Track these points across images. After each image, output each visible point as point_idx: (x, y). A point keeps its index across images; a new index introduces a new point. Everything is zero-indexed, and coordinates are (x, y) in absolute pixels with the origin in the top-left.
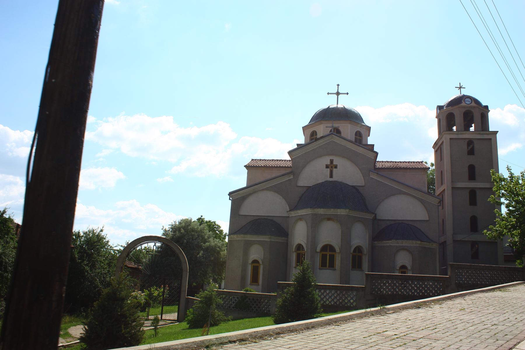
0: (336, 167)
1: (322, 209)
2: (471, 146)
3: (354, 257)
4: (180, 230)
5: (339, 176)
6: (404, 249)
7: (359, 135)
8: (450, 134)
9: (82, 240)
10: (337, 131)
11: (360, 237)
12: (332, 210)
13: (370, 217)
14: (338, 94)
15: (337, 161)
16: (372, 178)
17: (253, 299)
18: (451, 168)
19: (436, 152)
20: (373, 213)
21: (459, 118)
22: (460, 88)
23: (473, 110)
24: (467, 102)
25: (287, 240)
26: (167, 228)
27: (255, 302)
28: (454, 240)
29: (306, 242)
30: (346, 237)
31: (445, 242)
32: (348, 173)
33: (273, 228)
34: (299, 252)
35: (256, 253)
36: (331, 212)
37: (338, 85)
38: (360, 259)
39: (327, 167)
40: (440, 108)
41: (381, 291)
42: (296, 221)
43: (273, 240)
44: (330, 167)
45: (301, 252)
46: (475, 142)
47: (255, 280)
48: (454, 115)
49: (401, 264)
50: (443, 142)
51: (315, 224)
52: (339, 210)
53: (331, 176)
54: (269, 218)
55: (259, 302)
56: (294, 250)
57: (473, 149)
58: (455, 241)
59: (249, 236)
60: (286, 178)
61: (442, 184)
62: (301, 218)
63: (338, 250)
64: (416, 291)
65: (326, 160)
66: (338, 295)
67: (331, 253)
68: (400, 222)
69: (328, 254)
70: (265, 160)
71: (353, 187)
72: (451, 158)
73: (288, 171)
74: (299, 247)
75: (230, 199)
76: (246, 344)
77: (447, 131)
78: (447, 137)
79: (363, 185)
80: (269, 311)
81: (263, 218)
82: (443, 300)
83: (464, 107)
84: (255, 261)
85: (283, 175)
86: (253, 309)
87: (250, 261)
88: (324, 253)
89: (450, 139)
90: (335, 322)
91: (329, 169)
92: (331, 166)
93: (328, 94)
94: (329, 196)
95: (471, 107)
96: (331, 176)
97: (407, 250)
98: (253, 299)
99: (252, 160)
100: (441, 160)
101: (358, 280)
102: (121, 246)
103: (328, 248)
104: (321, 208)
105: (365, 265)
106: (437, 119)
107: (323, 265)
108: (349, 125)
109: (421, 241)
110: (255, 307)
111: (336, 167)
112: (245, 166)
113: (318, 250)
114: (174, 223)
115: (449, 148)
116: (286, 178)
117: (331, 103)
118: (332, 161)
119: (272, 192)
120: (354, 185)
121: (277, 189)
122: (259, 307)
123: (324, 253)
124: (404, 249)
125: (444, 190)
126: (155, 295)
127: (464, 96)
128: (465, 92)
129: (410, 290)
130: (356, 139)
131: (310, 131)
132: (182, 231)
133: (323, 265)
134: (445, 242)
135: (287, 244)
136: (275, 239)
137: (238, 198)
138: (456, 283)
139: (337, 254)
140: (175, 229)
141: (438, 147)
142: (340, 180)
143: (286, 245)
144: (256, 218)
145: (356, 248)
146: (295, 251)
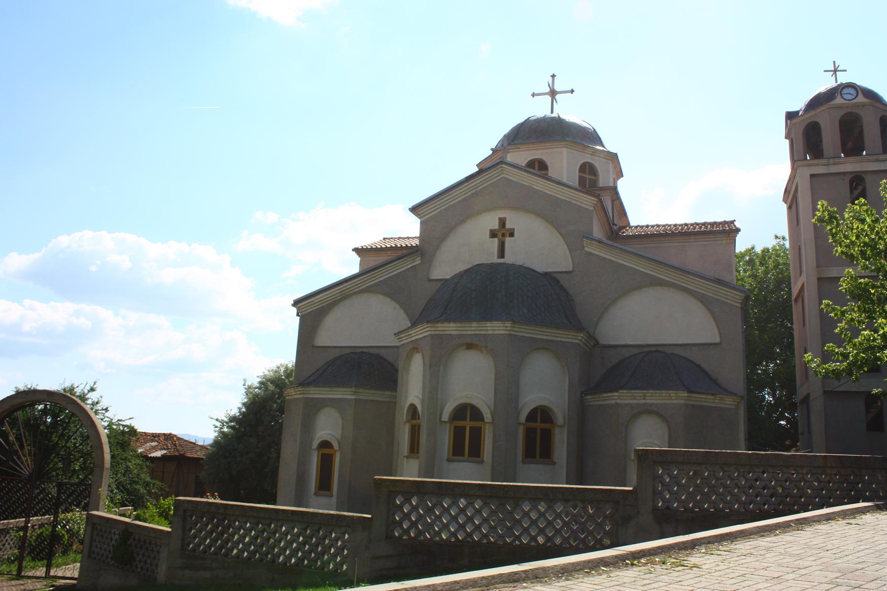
0: (512, 235)
1: (452, 325)
3: (530, 434)
5: (518, 253)
6: (649, 411)
7: (588, 170)
10: (539, 167)
11: (545, 384)
12: (474, 324)
14: (553, 93)
16: (590, 253)
17: (139, 541)
18: (816, 238)
19: (790, 208)
20: (579, 328)
21: (830, 137)
22: (835, 71)
23: (860, 112)
24: (845, 96)
25: (395, 397)
26: (255, 381)
29: (492, 404)
30: (508, 388)
31: (808, 396)
32: (537, 246)
33: (371, 370)
36: (472, 328)
37: (553, 76)
38: (547, 437)
39: (493, 234)
40: (790, 116)
42: (409, 357)
43: (362, 397)
44: (500, 235)
47: (324, 485)
52: (488, 324)
53: (502, 254)
54: (371, 351)
62: (415, 348)
63: (487, 416)
65: (491, 221)
67: (546, 426)
68: (654, 349)
69: (468, 424)
71: (546, 274)
74: (413, 409)
75: (298, 315)
78: (806, 172)
79: (571, 269)
82: (686, 549)
83: (840, 107)
84: (325, 444)
88: (461, 423)
89: (812, 176)
90: (785, 527)
91: (496, 240)
92: (502, 233)
93: (533, 95)
94: (496, 295)
95: (857, 105)
96: (502, 254)
97: (659, 415)
98: (145, 541)
102: (217, 420)
104: (449, 322)
106: (787, 141)
109: (690, 391)
111: (512, 235)
112: (357, 250)
113: (446, 417)
117: (540, 109)
118: (502, 222)
119: (381, 297)
120: (550, 270)
121: (392, 289)
123: (461, 423)
124: (649, 411)
126: (415, 498)
127: (842, 84)
128: (843, 78)
130: (582, 180)
132: (271, 387)
133: (457, 451)
134: (808, 396)
135: (395, 403)
136: (367, 395)
137: (313, 310)
138: (655, 509)
143: (391, 407)
144: (347, 351)
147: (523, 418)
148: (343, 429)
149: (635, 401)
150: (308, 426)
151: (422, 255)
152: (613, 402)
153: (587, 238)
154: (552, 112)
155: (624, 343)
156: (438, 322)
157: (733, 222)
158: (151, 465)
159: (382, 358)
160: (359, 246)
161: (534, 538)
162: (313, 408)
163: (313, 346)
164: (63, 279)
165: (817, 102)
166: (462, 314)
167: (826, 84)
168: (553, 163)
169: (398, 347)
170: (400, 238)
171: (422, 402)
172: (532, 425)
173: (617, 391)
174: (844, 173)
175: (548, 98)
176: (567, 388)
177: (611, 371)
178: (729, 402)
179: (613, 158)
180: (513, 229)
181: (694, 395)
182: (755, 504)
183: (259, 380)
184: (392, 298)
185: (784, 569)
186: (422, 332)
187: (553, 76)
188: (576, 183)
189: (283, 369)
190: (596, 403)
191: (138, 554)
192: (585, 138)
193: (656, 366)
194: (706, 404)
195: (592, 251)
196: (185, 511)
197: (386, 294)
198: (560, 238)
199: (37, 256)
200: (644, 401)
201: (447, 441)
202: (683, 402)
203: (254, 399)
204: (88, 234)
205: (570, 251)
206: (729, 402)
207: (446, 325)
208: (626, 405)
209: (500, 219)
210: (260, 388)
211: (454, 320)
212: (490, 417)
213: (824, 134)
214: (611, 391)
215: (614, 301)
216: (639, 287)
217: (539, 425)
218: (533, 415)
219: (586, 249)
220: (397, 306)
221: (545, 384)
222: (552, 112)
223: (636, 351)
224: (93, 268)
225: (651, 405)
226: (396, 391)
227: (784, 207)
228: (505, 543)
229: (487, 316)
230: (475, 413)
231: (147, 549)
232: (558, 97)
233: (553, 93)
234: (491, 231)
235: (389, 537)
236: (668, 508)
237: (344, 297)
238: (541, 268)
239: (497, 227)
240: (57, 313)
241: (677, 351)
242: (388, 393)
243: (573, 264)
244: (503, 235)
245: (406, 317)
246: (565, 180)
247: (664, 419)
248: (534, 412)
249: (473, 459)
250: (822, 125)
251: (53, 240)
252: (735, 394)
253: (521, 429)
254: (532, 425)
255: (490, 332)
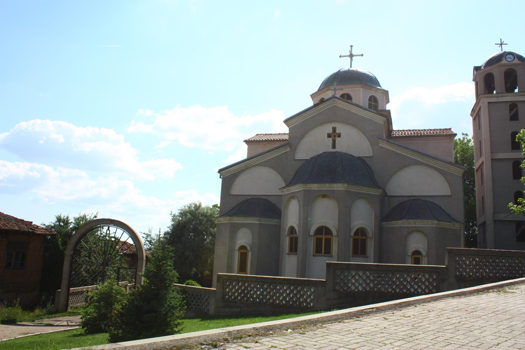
0: (339, 136)
1: (315, 185)
2: (515, 110)
3: (355, 241)
4: (186, 215)
6: (418, 230)
8: (488, 97)
9: (71, 226)
10: (347, 97)
11: (363, 216)
12: (327, 185)
13: (376, 192)
14: (351, 56)
15: (341, 128)
16: (382, 147)
17: (193, 295)
18: (490, 137)
19: (474, 119)
20: (379, 187)
21: (499, 81)
22: (501, 44)
23: (515, 68)
24: (508, 59)
25: (280, 222)
26: (177, 212)
27: (195, 298)
28: (494, 220)
29: (337, 227)
30: (345, 216)
31: (485, 222)
32: (353, 142)
33: (265, 208)
34: (292, 235)
35: (244, 238)
36: (326, 187)
37: (351, 46)
38: (364, 243)
39: (329, 136)
40: (477, 69)
41: (349, 287)
45: (294, 235)
46: (519, 105)
47: (242, 268)
48: (493, 76)
49: (414, 249)
50: (480, 108)
51: (308, 201)
52: (335, 185)
53: (334, 146)
54: (263, 197)
55: (199, 299)
56: (286, 234)
57: (511, 110)
58: (495, 221)
59: (235, 218)
60: (282, 151)
61: (481, 156)
62: (293, 196)
63: (334, 233)
64: (398, 286)
65: (328, 129)
66: (292, 291)
67: (363, 238)
68: (416, 198)
70: (271, 134)
71: (359, 158)
72: (490, 127)
73: (286, 142)
74: (292, 230)
75: (220, 177)
76: (237, 342)
77: (485, 94)
78: (485, 100)
79: (372, 155)
80: (208, 310)
81: (256, 197)
83: (504, 65)
84: (243, 247)
85: (278, 148)
86: (192, 308)
87: (237, 247)
89: (489, 103)
91: (331, 139)
92: (334, 135)
94: (329, 168)
96: (334, 146)
98: (197, 295)
99: (257, 135)
100: (479, 128)
101: (318, 271)
102: (144, 234)
103: (323, 230)
105: (371, 250)
106: (474, 82)
107: (318, 251)
108: (361, 89)
109: (439, 221)
110: (194, 305)
111: (339, 136)
112: (246, 141)
113: (312, 233)
114: (183, 208)
115: (487, 113)
116: (282, 151)
117: (344, 65)
118: (334, 129)
119: (267, 168)
121: (275, 165)
122: (198, 305)
124: (418, 230)
125: (483, 162)
127: (505, 52)
129: (391, 286)
130: (370, 106)
131: (320, 100)
132: (189, 216)
133: (318, 251)
134: (485, 222)
135: (280, 226)
136: (266, 221)
137: (229, 175)
138: (456, 275)
139: (334, 238)
140: (183, 214)
141: (476, 114)
142: (344, 151)
143: (278, 228)
144: (249, 198)
145: (358, 229)
146: (288, 235)
147: (352, 234)
148: (252, 239)
149: (410, 225)
150: (233, 237)
151: (290, 147)
152: (398, 225)
153: (381, 139)
154: (351, 67)
155: (400, 195)
156: (308, 183)
157: (450, 129)
158: (128, 259)
159: (269, 201)
160: (247, 138)
161: (401, 290)
162: (234, 229)
163: (230, 195)
164: (24, 148)
165: (492, 62)
166: (318, 178)
167: (496, 51)
168: (350, 94)
169: (281, 195)
170: (266, 134)
171: (299, 226)
172: (357, 237)
173: (401, 220)
174: (507, 102)
175: (349, 59)
176: (373, 218)
177: (399, 209)
178: (457, 226)
179: (386, 93)
180: (340, 133)
181: (440, 222)
182: (499, 274)
183: (179, 211)
184: (274, 169)
185: (338, 344)
186: (297, 188)
187: (351, 46)
188: (367, 107)
189: (193, 206)
190: (389, 226)
191: (192, 301)
192: (368, 81)
193: (416, 207)
194: (446, 227)
195: (383, 146)
196: (223, 279)
197: (270, 167)
198: (366, 138)
199: (7, 134)
200: (414, 225)
201: (334, 246)
202: (435, 226)
203: (189, 221)
204: (39, 121)
205: (371, 145)
206: (457, 226)
207: (312, 185)
208: (405, 227)
209: (333, 128)
210: (180, 216)
211: (317, 183)
212: (336, 233)
213: (495, 80)
214: (398, 220)
215: (395, 173)
216: (408, 166)
217: (360, 237)
218: (357, 233)
219: (380, 145)
220: (277, 174)
221: (363, 216)
222: (351, 67)
223: (406, 199)
224: (41, 142)
225: (418, 227)
226: (280, 219)
227: (471, 119)
228: (388, 291)
229: (334, 181)
230: (328, 231)
231: (199, 299)
232: (354, 58)
233: (351, 56)
234: (328, 134)
235: (334, 290)
236: (461, 275)
237: (247, 168)
238: (356, 155)
239: (331, 132)
240: (19, 168)
241: (428, 199)
242: (276, 220)
243: (373, 152)
244: (335, 136)
245: (282, 179)
246: (361, 104)
247: (425, 234)
248: (358, 230)
249: (326, 255)
250: (494, 74)
251: (17, 125)
252: (459, 222)
253: (351, 239)
254: (357, 237)
255: (336, 189)
